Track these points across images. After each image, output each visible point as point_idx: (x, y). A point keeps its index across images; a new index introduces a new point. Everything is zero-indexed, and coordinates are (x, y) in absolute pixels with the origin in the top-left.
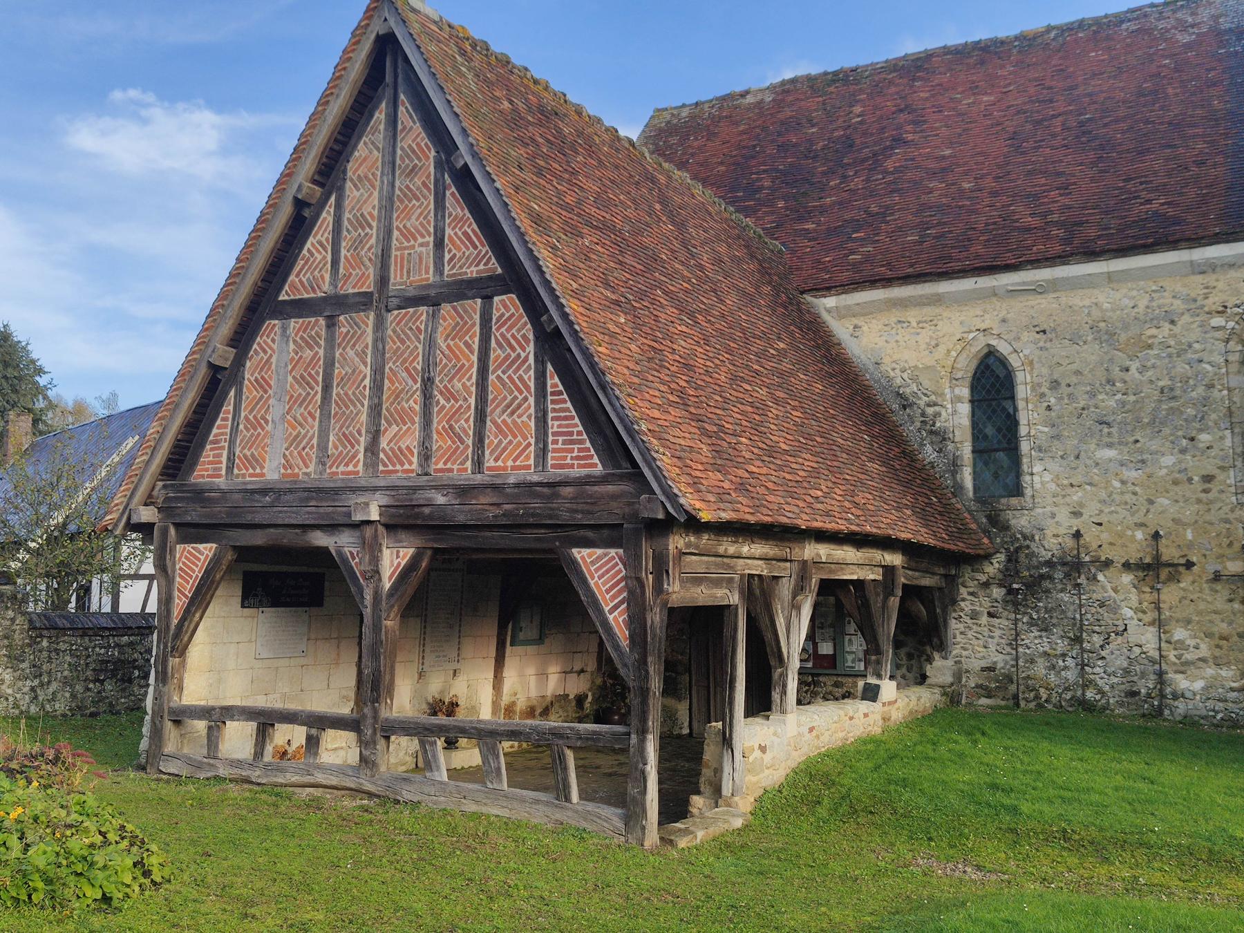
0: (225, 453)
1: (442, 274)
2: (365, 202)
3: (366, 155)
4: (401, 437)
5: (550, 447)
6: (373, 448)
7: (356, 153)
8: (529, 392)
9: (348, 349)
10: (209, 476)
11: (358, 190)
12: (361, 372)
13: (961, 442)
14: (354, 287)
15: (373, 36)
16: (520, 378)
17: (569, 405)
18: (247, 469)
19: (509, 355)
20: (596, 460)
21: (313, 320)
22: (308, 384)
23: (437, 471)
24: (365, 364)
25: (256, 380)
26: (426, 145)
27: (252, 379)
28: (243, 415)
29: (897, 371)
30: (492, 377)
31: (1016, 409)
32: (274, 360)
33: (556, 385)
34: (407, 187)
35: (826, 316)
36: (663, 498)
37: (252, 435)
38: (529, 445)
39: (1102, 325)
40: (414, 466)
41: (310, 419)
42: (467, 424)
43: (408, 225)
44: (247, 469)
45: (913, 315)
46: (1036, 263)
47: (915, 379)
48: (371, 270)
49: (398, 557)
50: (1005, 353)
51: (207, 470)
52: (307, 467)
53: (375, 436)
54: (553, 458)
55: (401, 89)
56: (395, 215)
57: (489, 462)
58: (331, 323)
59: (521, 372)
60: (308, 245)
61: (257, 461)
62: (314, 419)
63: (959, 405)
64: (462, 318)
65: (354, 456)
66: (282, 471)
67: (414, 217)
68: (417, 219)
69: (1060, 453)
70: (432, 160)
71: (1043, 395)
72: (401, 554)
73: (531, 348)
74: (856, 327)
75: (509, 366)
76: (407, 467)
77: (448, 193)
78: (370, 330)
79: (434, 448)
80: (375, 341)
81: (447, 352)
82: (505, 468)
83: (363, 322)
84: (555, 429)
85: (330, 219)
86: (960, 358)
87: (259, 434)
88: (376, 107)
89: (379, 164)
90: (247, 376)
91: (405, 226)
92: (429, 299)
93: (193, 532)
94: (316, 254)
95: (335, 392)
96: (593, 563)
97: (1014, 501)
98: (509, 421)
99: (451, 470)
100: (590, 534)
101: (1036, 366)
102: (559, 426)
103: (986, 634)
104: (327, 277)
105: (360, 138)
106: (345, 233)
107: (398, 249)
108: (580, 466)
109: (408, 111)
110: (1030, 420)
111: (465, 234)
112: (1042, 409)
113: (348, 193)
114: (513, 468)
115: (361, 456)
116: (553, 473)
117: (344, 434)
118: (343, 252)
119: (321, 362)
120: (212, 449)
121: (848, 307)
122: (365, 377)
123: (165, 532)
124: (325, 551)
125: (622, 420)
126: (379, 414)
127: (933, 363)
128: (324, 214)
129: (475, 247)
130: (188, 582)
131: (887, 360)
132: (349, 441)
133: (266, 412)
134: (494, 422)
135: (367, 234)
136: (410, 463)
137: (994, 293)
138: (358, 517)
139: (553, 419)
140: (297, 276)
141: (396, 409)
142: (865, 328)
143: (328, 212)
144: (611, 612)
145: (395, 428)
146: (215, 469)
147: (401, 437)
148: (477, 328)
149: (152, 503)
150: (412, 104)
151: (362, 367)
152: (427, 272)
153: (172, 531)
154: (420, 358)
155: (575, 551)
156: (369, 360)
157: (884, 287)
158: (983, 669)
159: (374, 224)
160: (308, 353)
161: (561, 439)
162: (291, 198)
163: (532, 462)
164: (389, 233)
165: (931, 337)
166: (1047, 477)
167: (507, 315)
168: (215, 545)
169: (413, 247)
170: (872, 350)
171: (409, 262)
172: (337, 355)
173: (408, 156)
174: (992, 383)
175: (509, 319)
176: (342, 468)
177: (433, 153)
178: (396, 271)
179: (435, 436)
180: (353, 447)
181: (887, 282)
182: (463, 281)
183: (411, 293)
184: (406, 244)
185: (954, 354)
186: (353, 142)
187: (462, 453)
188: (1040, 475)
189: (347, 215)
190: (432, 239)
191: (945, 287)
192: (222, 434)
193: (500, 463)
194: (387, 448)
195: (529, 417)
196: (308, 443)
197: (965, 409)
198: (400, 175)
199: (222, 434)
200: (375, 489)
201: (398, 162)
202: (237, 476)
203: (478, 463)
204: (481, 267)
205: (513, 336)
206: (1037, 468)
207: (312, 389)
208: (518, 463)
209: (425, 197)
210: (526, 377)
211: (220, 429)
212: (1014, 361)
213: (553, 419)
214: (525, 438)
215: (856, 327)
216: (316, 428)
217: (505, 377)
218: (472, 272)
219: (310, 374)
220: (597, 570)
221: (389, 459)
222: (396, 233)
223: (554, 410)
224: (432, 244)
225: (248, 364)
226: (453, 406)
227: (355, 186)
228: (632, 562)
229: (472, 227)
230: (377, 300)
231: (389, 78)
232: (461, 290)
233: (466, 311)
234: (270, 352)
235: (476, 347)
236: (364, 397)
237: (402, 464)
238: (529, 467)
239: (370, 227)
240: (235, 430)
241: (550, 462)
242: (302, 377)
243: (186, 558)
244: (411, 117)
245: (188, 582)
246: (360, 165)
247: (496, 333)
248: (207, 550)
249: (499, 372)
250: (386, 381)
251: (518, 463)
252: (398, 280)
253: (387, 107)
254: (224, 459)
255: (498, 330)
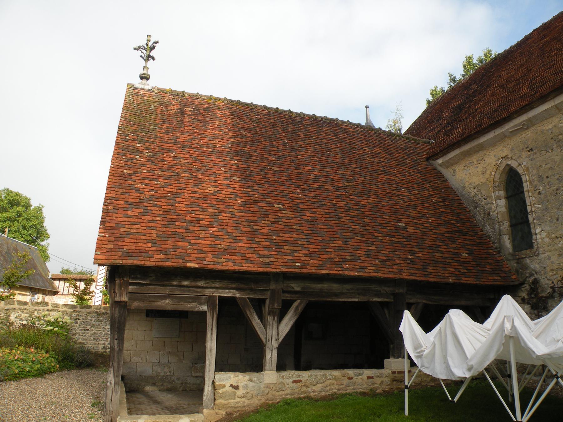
35: (439, 168)
45: (475, 158)
63: (499, 201)
86: (496, 175)
112: (536, 195)
121: (447, 161)
127: (485, 181)
131: (467, 184)
165: (483, 168)
185: (493, 173)
188: (541, 234)
197: (502, 202)
206: (538, 231)
212: (520, 171)
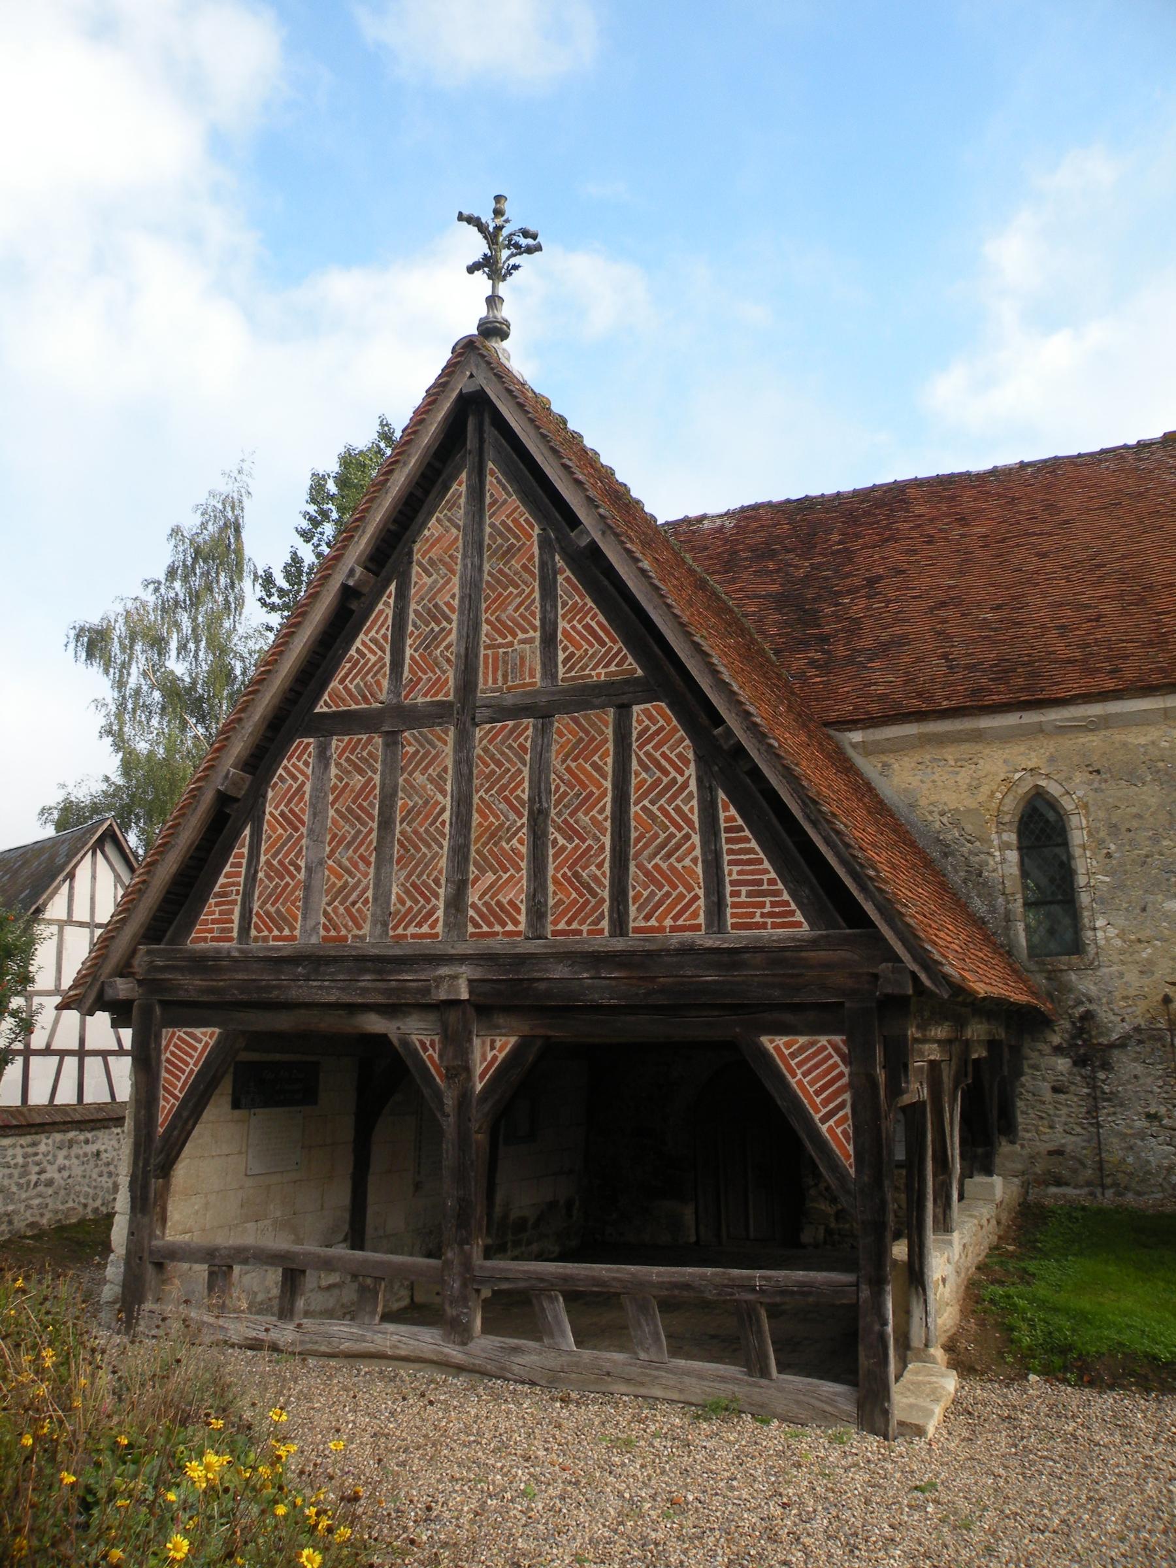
0: (237, 910)
1: (554, 676)
2: (440, 590)
3: (441, 532)
4: (499, 889)
5: (729, 900)
6: (456, 903)
7: (426, 532)
8: (693, 829)
9: (417, 774)
10: (213, 939)
11: (430, 575)
12: (437, 803)
13: (1013, 894)
14: (425, 695)
15: (454, 395)
16: (678, 809)
17: (753, 844)
18: (270, 931)
19: (659, 780)
20: (799, 917)
21: (365, 737)
22: (358, 818)
23: (556, 933)
24: (443, 792)
25: (282, 814)
26: (526, 520)
27: (276, 813)
28: (263, 859)
29: (936, 815)
30: (634, 809)
31: (1070, 857)
32: (307, 788)
33: (733, 819)
34: (500, 571)
35: (851, 753)
36: (914, 967)
37: (276, 887)
38: (696, 898)
39: (1161, 764)
40: (522, 927)
41: (361, 865)
42: (601, 871)
43: (504, 617)
44: (270, 931)
45: (950, 753)
46: (1087, 698)
47: (956, 824)
48: (451, 674)
49: (493, 1048)
50: (1056, 795)
51: (211, 931)
52: (360, 928)
53: (460, 888)
54: (733, 915)
55: (490, 452)
56: (484, 606)
57: (635, 918)
58: (392, 740)
59: (678, 802)
60: (358, 643)
61: (285, 919)
62: (368, 864)
64: (587, 733)
65: (431, 913)
66: (322, 933)
67: (511, 608)
68: (516, 610)
69: (1125, 905)
70: (535, 537)
71: (1101, 842)
72: (498, 1044)
73: (691, 771)
74: (885, 765)
75: (661, 795)
76: (510, 927)
77: (560, 579)
78: (449, 749)
79: (551, 902)
80: (457, 763)
81: (567, 776)
82: (661, 929)
83: (440, 739)
84: (735, 877)
85: (390, 612)
86: (1006, 801)
87: (287, 884)
88: (453, 477)
89: (460, 543)
90: (268, 810)
91: (498, 619)
92: (542, 711)
93: (188, 1012)
94: (369, 655)
95: (398, 829)
96: (793, 1055)
97: (1074, 959)
98: (664, 866)
99: (578, 932)
100: (788, 1018)
101: (1092, 809)
102: (739, 873)
103: (1051, 1112)
104: (385, 683)
105: (430, 514)
106: (410, 628)
107: (487, 647)
108: (775, 926)
109: (499, 482)
110: (1088, 869)
111: (587, 627)
112: (1100, 857)
113: (414, 579)
114: (674, 929)
115: (440, 913)
116: (734, 937)
117: (414, 885)
118: (408, 652)
119: (377, 791)
120: (217, 904)
121: (876, 743)
122: (443, 810)
123: (147, 1011)
124: (383, 1038)
125: (843, 862)
126: (466, 858)
128: (380, 606)
129: (603, 644)
130: (179, 1079)
131: (923, 802)
132: (422, 894)
133: (298, 855)
134: (639, 866)
135: (443, 629)
136: (516, 923)
137: (1040, 729)
138: (443, 995)
139: (730, 863)
140: (342, 682)
141: (491, 851)
142: (896, 766)
143: (387, 604)
144: (824, 1120)
145: (490, 877)
146: (223, 930)
147: (499, 889)
148: (610, 745)
149: (132, 974)
150: (504, 474)
151: (440, 797)
152: (532, 676)
153: (158, 1010)
154: (526, 784)
155: (764, 1039)
156: (448, 788)
157: (917, 721)
158: (1050, 1153)
159: (454, 617)
160: (358, 780)
161: (744, 890)
162: (338, 585)
163: (701, 920)
164: (476, 627)
166: (1112, 932)
167: (654, 728)
168: (217, 1030)
169: (511, 644)
170: (906, 790)
171: (505, 663)
172: (401, 780)
173: (501, 534)
174: (1040, 828)
175: (657, 732)
176: (412, 930)
177: (537, 530)
178: (486, 674)
179: (551, 888)
180: (428, 901)
181: (920, 716)
182: (585, 686)
183: (509, 700)
184: (500, 640)
186: (420, 518)
187: (594, 909)
188: (1104, 930)
189: (413, 606)
190: (538, 634)
191: (986, 723)
192: (233, 884)
193: (653, 922)
194: (479, 904)
195: (694, 860)
196: (360, 897)
197: (1013, 856)
198: (490, 557)
199: (233, 884)
200: (462, 959)
201: (487, 541)
202: (256, 939)
203: (619, 925)
204: (613, 668)
205: (664, 755)
207: (364, 824)
208: (680, 922)
209: (525, 583)
210: (686, 809)
211: (230, 876)
212: (1068, 804)
213: (730, 863)
214: (690, 889)
215: (885, 765)
216: (371, 876)
217: (654, 809)
218: (600, 674)
219: (360, 807)
220: (799, 1065)
221: (482, 915)
222: (485, 628)
223: (731, 852)
224: (537, 643)
225: (270, 794)
226: (577, 847)
227: (425, 570)
228: (857, 1056)
229: (597, 619)
230: (463, 710)
231: (471, 442)
232: (583, 697)
233: (593, 725)
234: (301, 778)
235: (609, 769)
236: (443, 835)
237: (504, 925)
238: (697, 928)
239: (449, 621)
240: (251, 878)
241: (730, 921)
242: (349, 809)
243: (176, 1046)
244: (504, 488)
245: (179, 1079)
246: (433, 545)
247: (638, 753)
248: (205, 1037)
249: (646, 802)
250: (475, 815)
251: (680, 922)
252: (487, 684)
253: (469, 478)
254: (236, 916)
255: (641, 747)
